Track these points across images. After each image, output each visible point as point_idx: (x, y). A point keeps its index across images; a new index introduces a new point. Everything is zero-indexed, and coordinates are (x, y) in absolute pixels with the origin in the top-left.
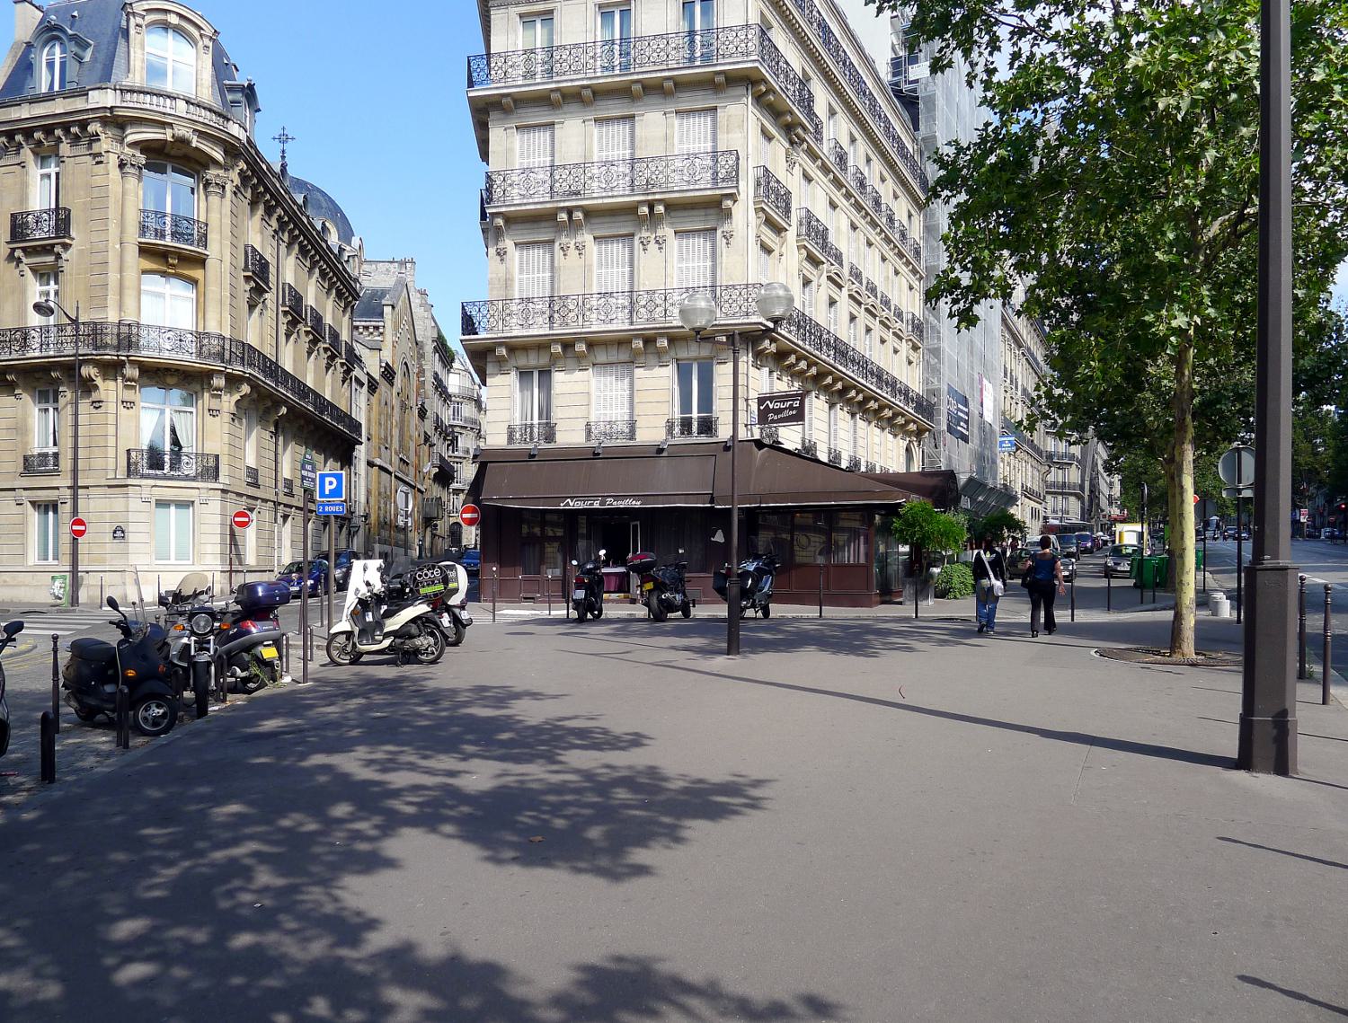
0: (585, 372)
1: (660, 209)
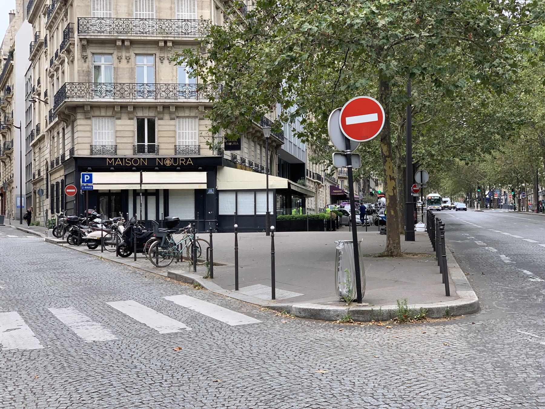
0: (132, 121)
1: (170, 44)
